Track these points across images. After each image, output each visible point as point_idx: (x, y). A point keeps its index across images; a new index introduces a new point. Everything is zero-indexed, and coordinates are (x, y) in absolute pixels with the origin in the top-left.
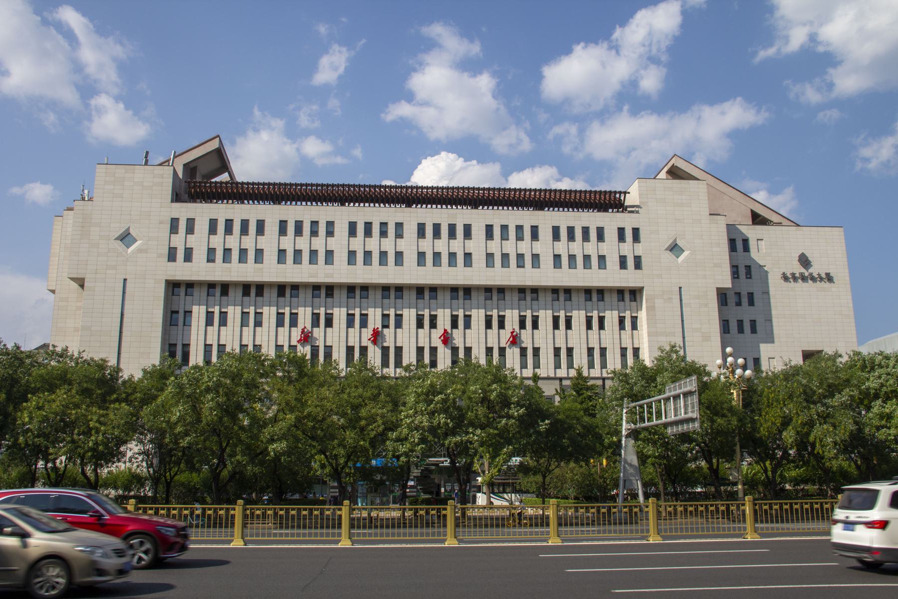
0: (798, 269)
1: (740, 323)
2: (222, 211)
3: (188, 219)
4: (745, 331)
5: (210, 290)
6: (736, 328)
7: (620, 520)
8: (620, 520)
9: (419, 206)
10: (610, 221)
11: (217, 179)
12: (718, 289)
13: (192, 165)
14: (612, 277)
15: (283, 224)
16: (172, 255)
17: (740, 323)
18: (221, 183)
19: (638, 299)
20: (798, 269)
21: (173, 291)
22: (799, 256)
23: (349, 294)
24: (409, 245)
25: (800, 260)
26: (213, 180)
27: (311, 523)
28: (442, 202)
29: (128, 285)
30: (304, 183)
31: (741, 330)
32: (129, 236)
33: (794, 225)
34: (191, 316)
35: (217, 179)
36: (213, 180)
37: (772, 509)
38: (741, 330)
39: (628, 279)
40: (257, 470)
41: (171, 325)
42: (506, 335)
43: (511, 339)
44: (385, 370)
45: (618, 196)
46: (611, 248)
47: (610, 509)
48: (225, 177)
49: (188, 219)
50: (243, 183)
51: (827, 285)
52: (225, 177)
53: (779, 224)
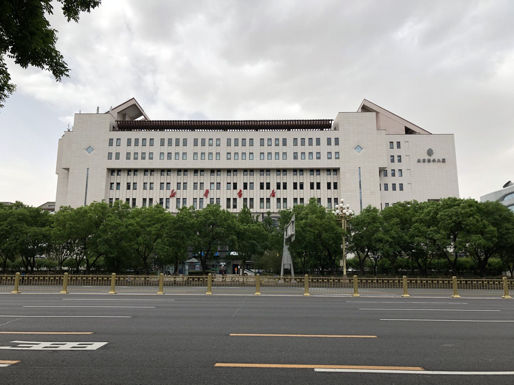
0: (427, 157)
1: (394, 185)
2: (134, 134)
3: (135, 139)
4: (396, 189)
5: (179, 173)
6: (392, 188)
7: (134, 283)
8: (134, 283)
9: (317, 130)
10: (323, 134)
11: (139, 119)
12: (339, 168)
13: (124, 112)
14: (324, 163)
15: (229, 140)
16: (110, 155)
17: (394, 185)
18: (140, 121)
19: (338, 174)
20: (427, 157)
21: (167, 174)
22: (428, 151)
23: (195, 174)
24: (223, 149)
25: (428, 151)
26: (136, 120)
27: (124, 283)
28: (247, 128)
29: (89, 171)
30: (221, 120)
31: (394, 189)
32: (361, 149)
33: (429, 134)
34: (120, 185)
35: (139, 119)
36: (136, 120)
37: (378, 283)
38: (394, 189)
39: (332, 164)
40: (469, 259)
41: (167, 189)
42: (269, 192)
43: (272, 194)
44: (229, 210)
45: (330, 122)
46: (324, 148)
47: (399, 281)
48: (141, 118)
49: (135, 139)
50: (153, 121)
51: (441, 164)
52: (141, 118)
53: (419, 134)
